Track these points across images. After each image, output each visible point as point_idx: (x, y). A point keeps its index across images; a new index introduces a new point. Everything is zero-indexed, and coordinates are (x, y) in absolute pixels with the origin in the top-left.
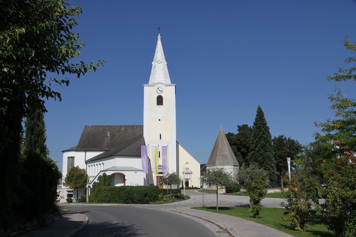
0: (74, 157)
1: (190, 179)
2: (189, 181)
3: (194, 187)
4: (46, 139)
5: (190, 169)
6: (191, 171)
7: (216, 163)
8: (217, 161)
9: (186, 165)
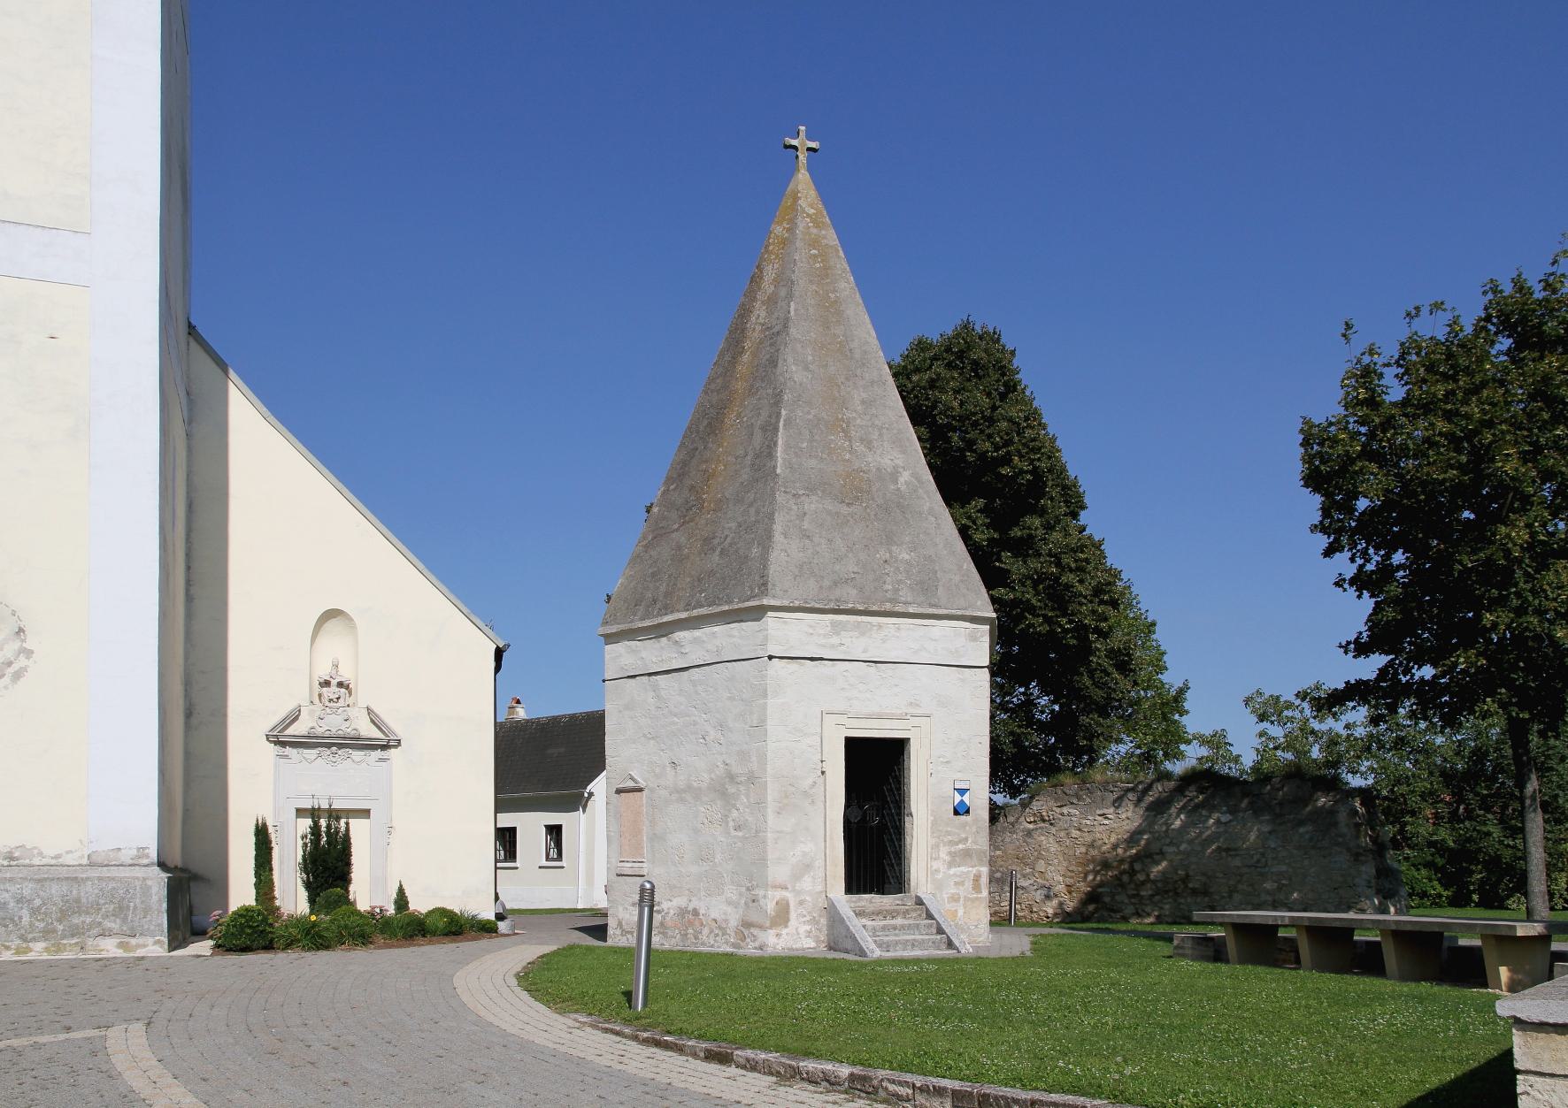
0: (1247, 701)
1: (365, 813)
2: (359, 833)
3: (420, 904)
4: (992, 783)
5: (364, 696)
6: (376, 722)
7: (773, 570)
8: (784, 554)
9: (323, 640)
